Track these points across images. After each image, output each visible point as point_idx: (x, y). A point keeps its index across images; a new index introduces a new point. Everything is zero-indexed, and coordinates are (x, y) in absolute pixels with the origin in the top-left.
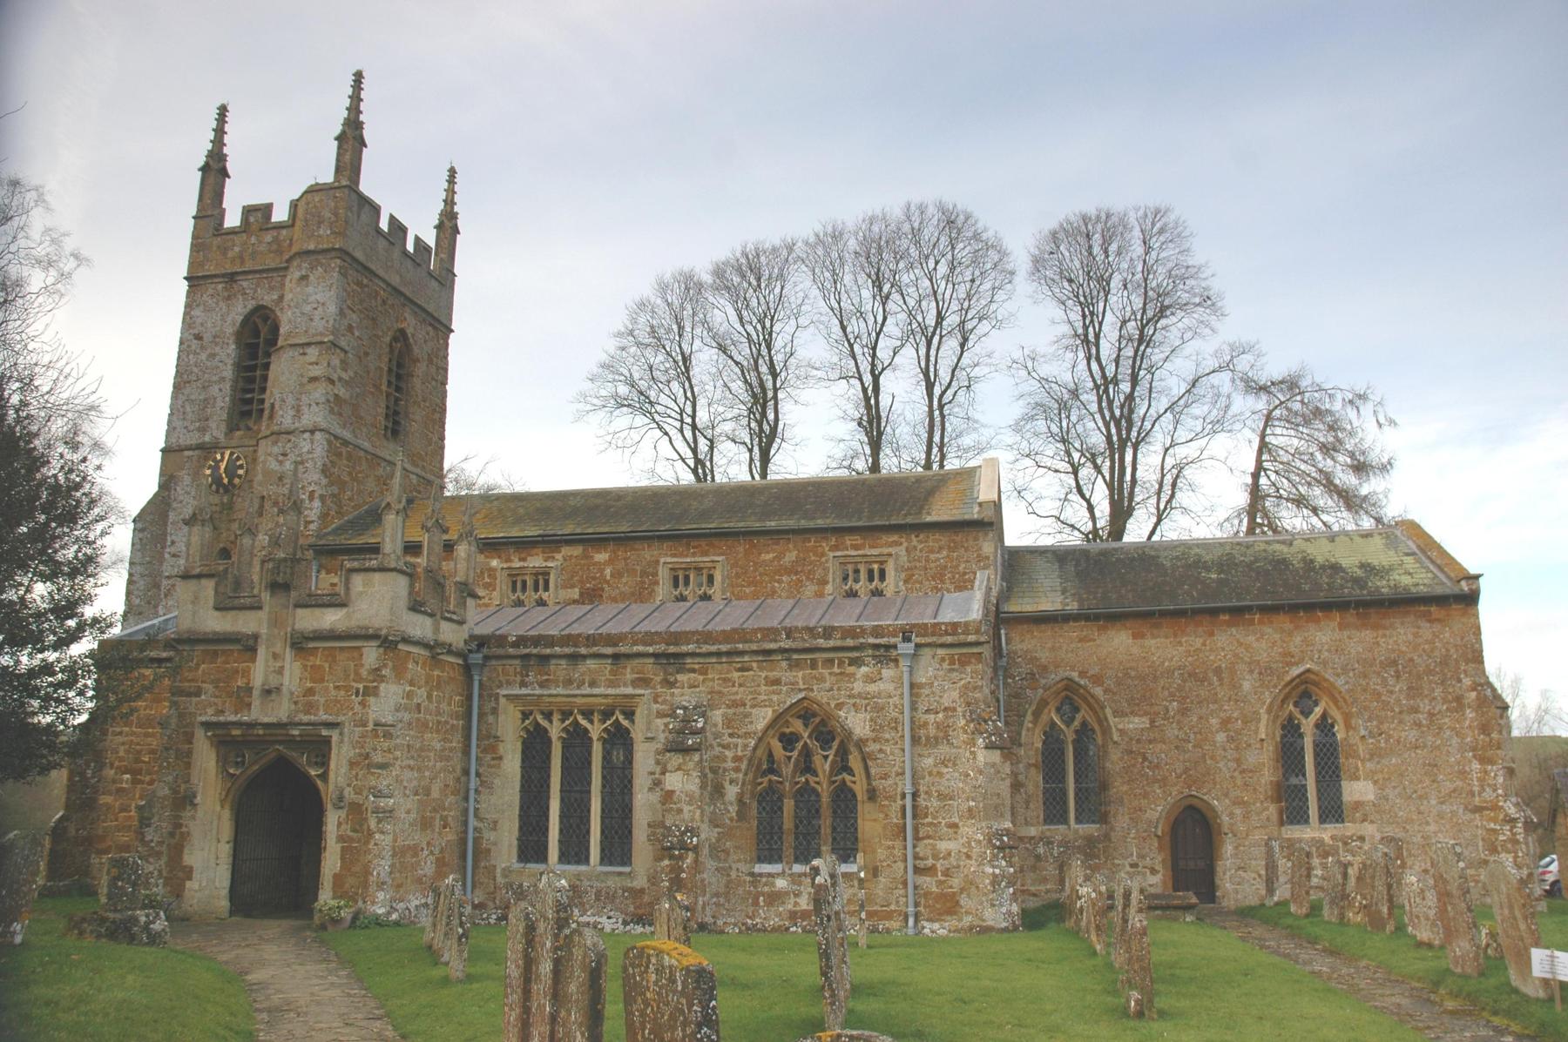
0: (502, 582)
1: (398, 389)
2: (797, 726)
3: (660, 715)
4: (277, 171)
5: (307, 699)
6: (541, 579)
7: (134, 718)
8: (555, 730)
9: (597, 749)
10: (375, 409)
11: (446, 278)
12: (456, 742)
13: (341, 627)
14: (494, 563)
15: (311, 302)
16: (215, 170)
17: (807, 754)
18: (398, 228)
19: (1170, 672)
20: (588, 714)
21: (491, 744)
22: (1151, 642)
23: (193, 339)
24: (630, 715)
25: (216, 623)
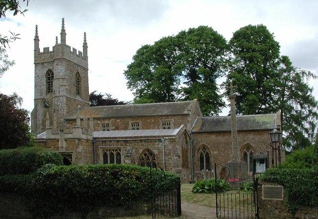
0: (101, 126)
1: (78, 84)
2: (147, 152)
3: (125, 150)
4: (48, 42)
5: (67, 148)
6: (108, 125)
7: (259, 182)
8: (108, 153)
9: (115, 156)
10: (74, 90)
11: (85, 58)
12: (92, 155)
13: (72, 137)
14: (99, 122)
15: (60, 70)
16: (37, 40)
17: (148, 157)
18: (75, 50)
19: (222, 143)
20: (113, 150)
21: (98, 155)
22: (219, 137)
23: (37, 77)
24: (120, 150)
25: (53, 137)
